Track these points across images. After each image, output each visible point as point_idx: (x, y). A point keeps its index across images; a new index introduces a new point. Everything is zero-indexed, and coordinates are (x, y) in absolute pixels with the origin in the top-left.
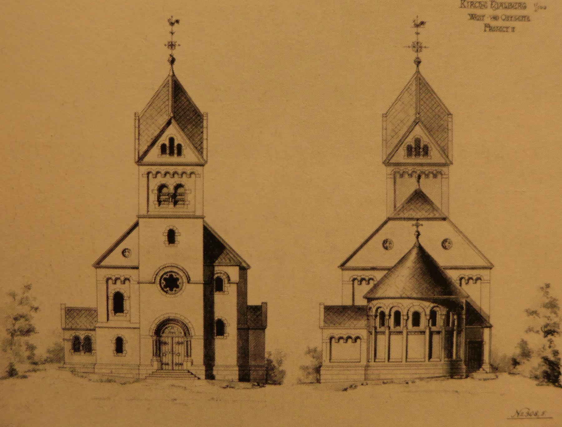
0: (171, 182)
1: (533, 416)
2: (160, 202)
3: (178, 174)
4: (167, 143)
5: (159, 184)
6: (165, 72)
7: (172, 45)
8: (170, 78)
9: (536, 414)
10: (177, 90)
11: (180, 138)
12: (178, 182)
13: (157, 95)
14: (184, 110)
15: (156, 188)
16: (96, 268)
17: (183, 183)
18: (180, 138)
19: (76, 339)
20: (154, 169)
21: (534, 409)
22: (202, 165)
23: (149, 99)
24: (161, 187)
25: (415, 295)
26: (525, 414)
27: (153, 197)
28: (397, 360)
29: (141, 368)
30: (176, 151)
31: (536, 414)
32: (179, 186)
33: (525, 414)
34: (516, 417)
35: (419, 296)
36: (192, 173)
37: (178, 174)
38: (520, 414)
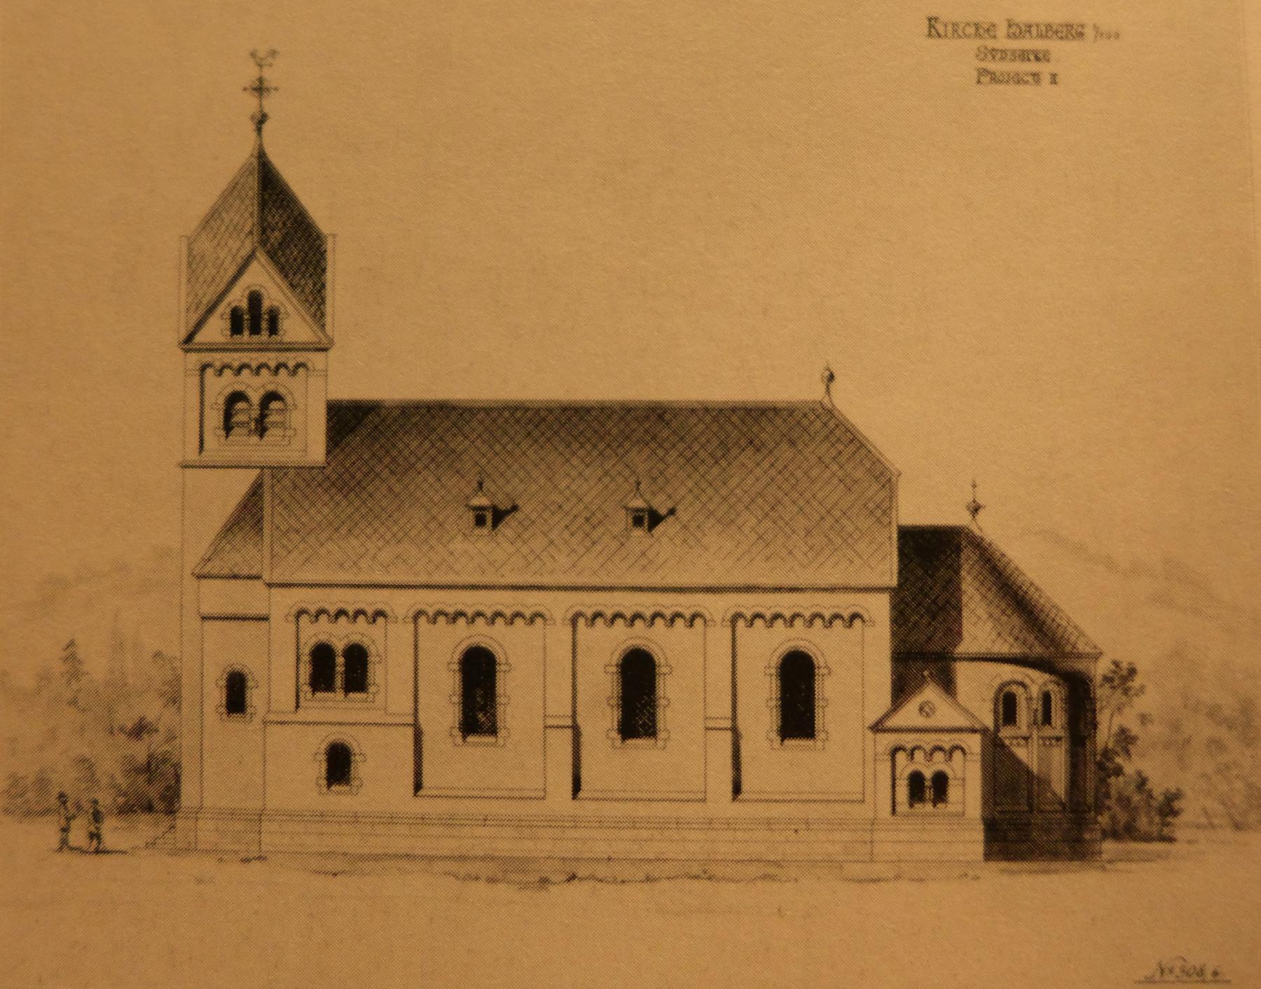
0: (255, 387)
1: (1195, 977)
2: (228, 427)
3: (269, 368)
4: (244, 304)
5: (229, 391)
6: (240, 154)
7: (260, 89)
8: (255, 162)
9: (1201, 972)
10: (270, 187)
11: (275, 292)
12: (271, 388)
13: (234, 187)
14: (283, 226)
15: (221, 400)
16: (187, 351)
17: (282, 391)
18: (275, 292)
19: (916, 780)
20: (218, 358)
21: (1194, 961)
22: (325, 350)
23: (215, 199)
24: (236, 397)
25: (1002, 648)
26: (1177, 971)
27: (214, 418)
28: (692, 796)
29: (265, 826)
30: (264, 325)
31: (1201, 972)
32: (272, 396)
33: (1177, 971)
34: (1157, 977)
35: (1017, 650)
36: (298, 366)
37: (269, 368)
38: (1167, 971)
